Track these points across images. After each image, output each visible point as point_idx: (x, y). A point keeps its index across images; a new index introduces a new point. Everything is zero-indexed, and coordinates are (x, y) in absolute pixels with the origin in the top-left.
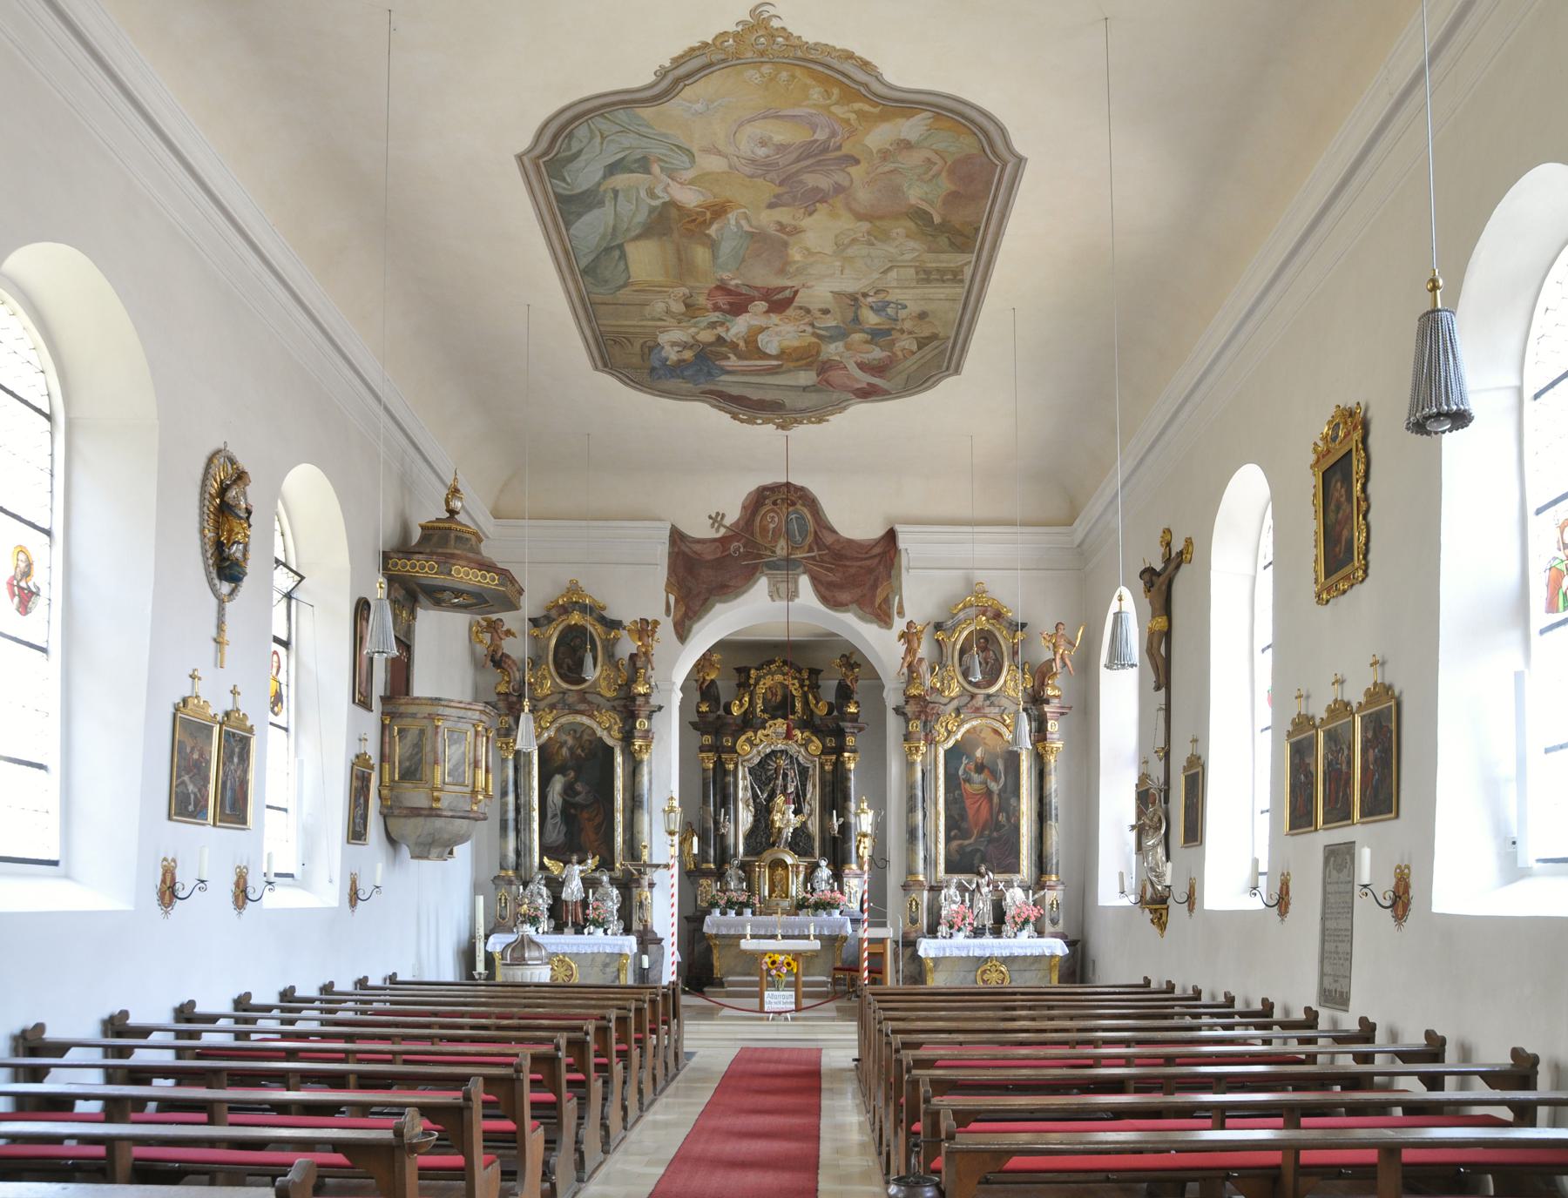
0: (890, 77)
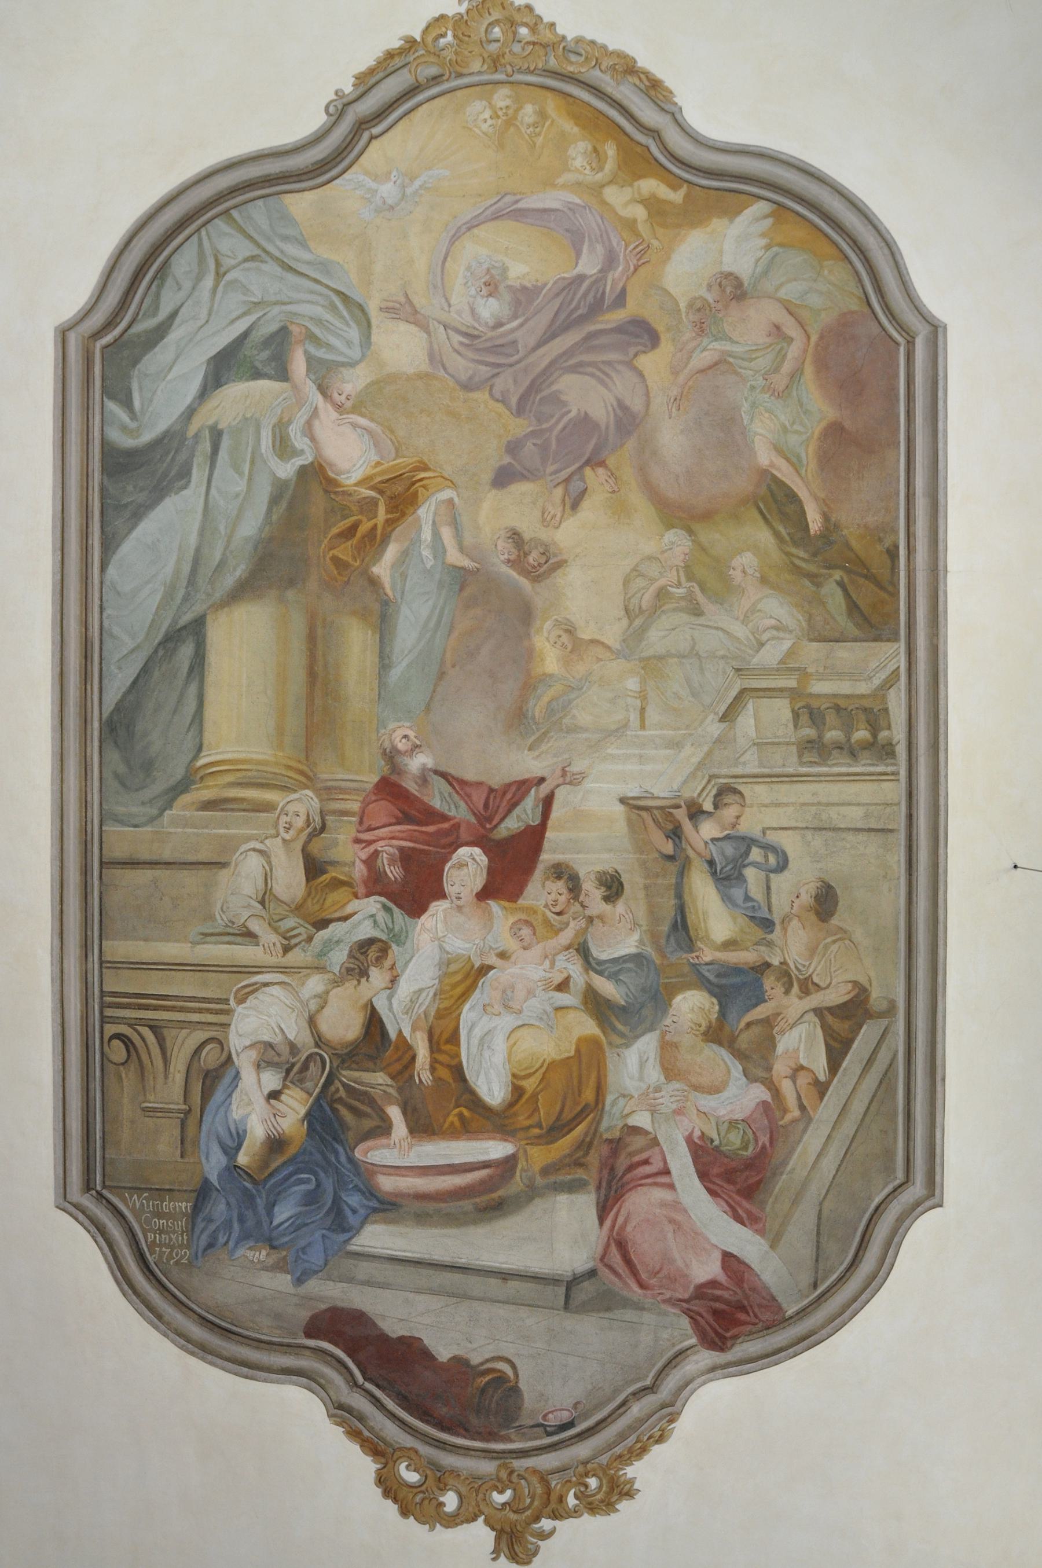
0: (695, 118)
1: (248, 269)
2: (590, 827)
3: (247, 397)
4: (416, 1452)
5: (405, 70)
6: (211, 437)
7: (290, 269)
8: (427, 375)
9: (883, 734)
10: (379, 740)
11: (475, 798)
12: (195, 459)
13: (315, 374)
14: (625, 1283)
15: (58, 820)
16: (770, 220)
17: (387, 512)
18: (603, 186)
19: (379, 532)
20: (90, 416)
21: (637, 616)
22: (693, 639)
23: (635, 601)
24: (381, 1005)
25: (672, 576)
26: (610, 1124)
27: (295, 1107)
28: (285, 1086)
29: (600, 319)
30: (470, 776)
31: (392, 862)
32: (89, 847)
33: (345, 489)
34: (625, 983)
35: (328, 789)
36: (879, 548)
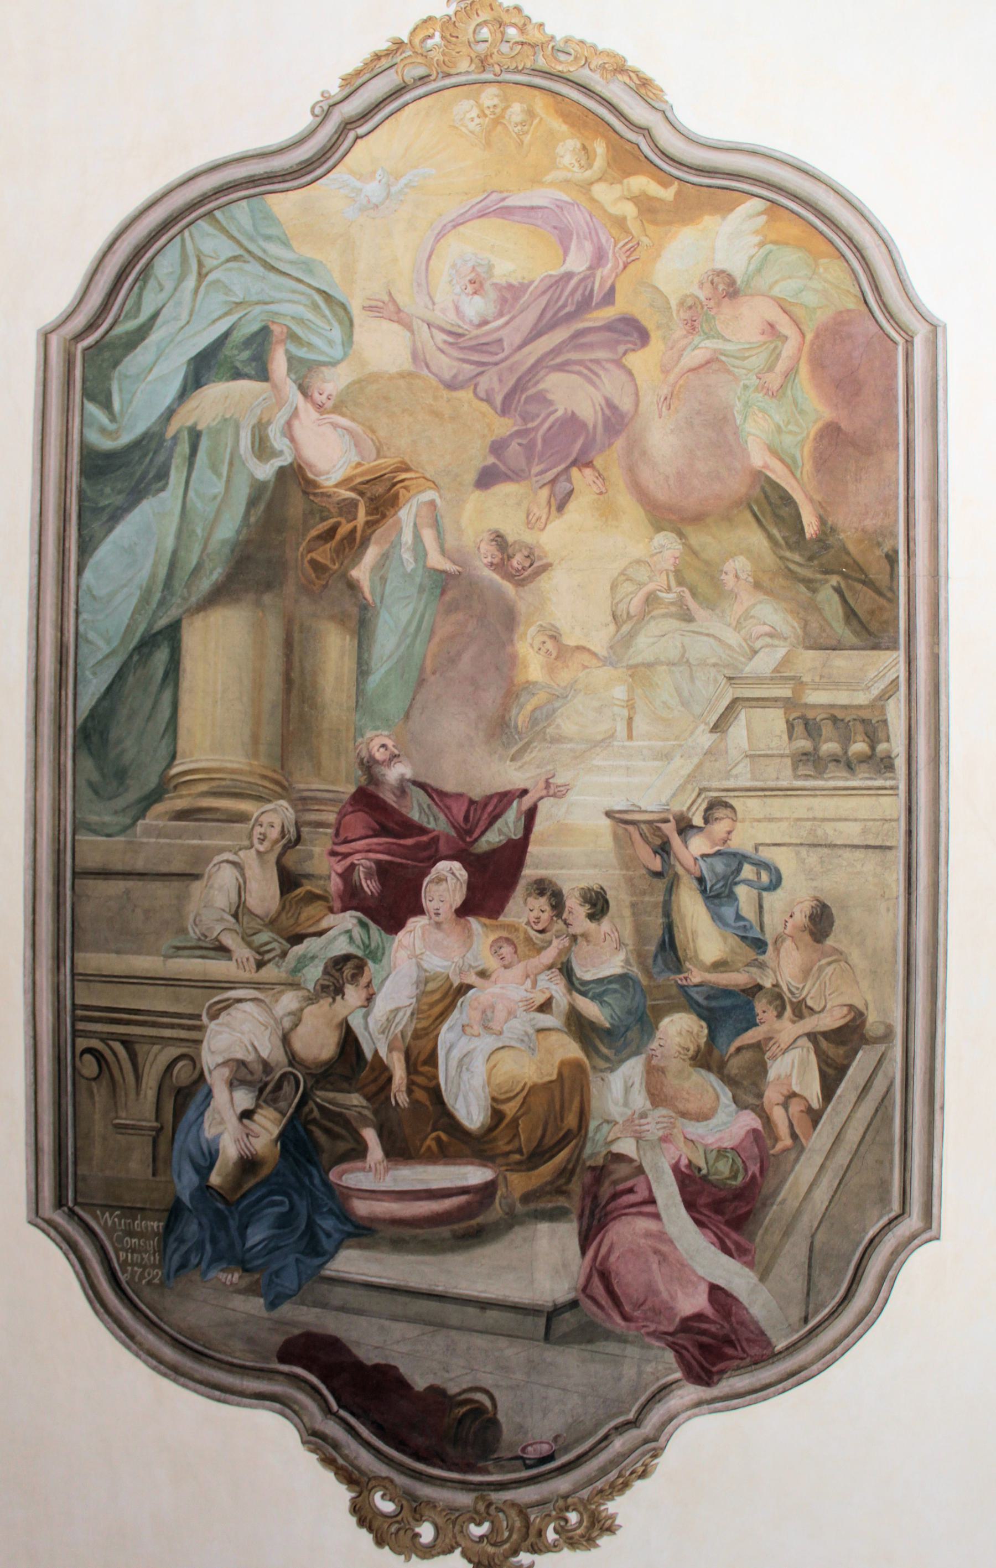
1: (230, 270)
2: (575, 842)
3: (227, 397)
4: (392, 1481)
5: (392, 71)
6: (190, 438)
7: (273, 269)
8: (410, 374)
9: (882, 747)
10: (356, 748)
11: (455, 811)
12: (173, 461)
13: (296, 373)
14: (608, 1315)
15: (31, 828)
16: (764, 218)
17: (368, 514)
18: (592, 183)
19: (358, 535)
20: (70, 418)
21: (624, 622)
22: (683, 646)
23: (623, 606)
24: (356, 1023)
25: (662, 580)
26: (594, 1151)
27: (268, 1128)
28: (258, 1106)
29: (589, 316)
30: (450, 786)
31: (369, 876)
32: (62, 856)
33: (324, 490)
34: (610, 1005)
35: (304, 799)
36: (878, 552)
